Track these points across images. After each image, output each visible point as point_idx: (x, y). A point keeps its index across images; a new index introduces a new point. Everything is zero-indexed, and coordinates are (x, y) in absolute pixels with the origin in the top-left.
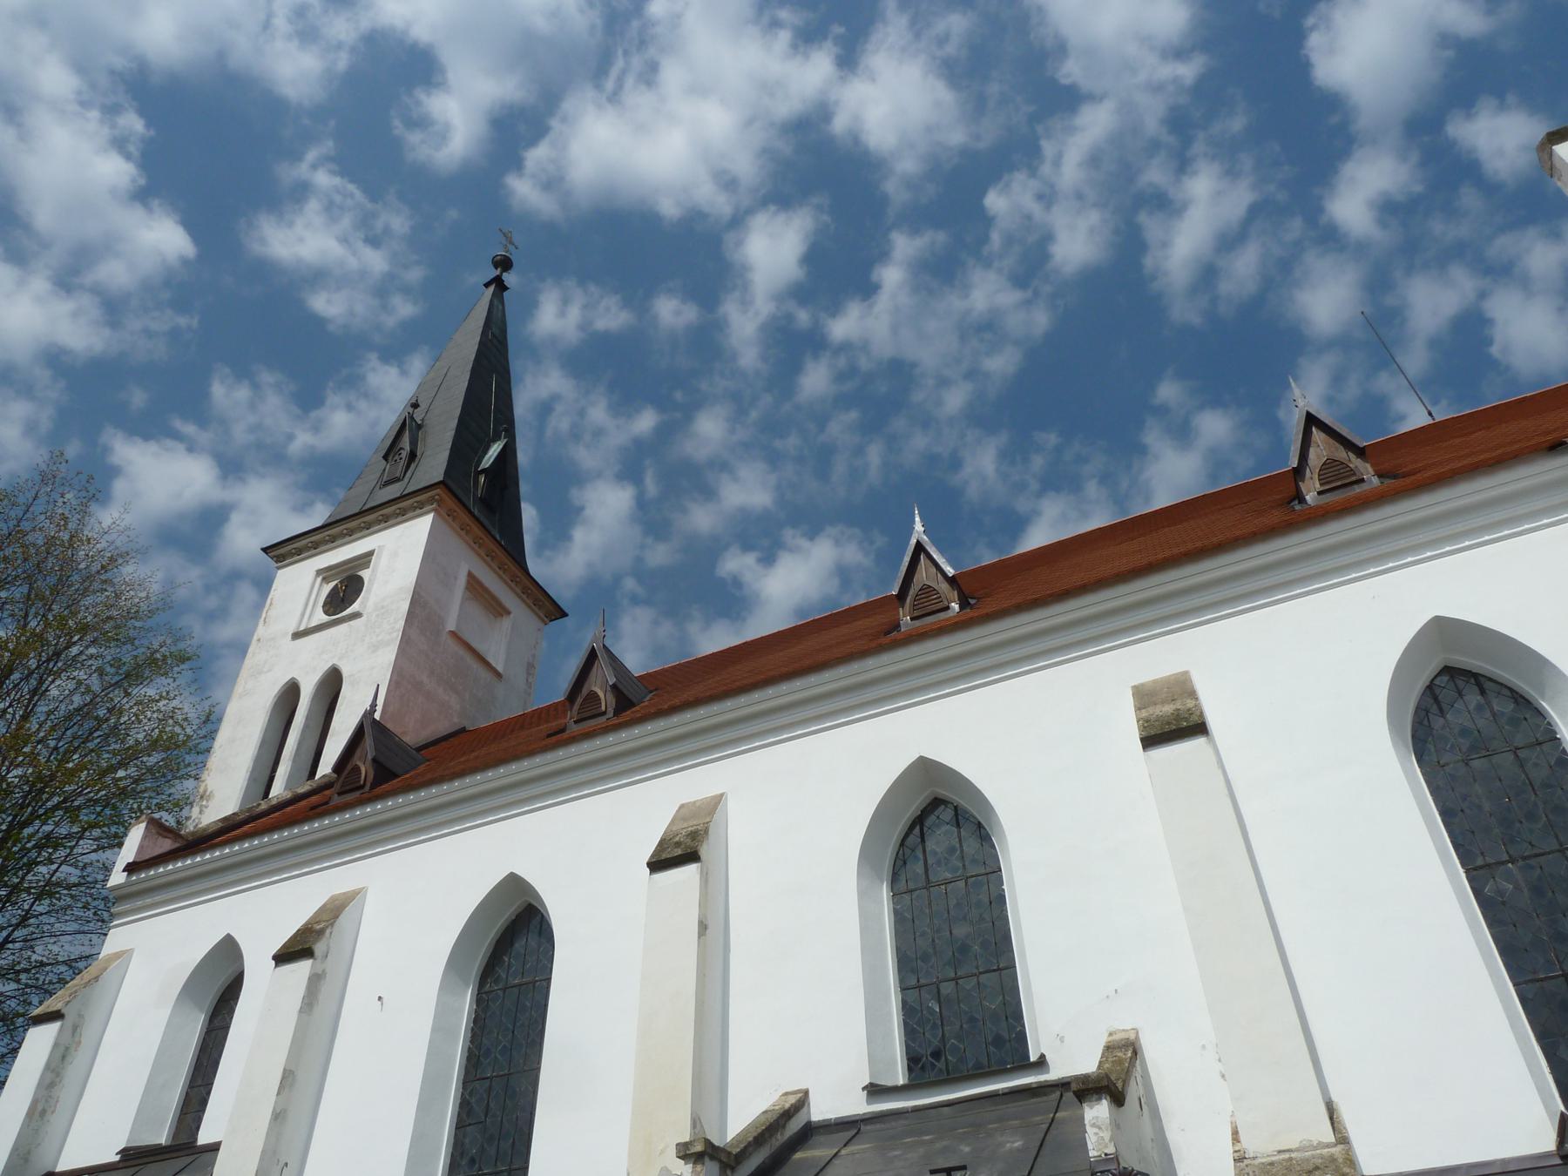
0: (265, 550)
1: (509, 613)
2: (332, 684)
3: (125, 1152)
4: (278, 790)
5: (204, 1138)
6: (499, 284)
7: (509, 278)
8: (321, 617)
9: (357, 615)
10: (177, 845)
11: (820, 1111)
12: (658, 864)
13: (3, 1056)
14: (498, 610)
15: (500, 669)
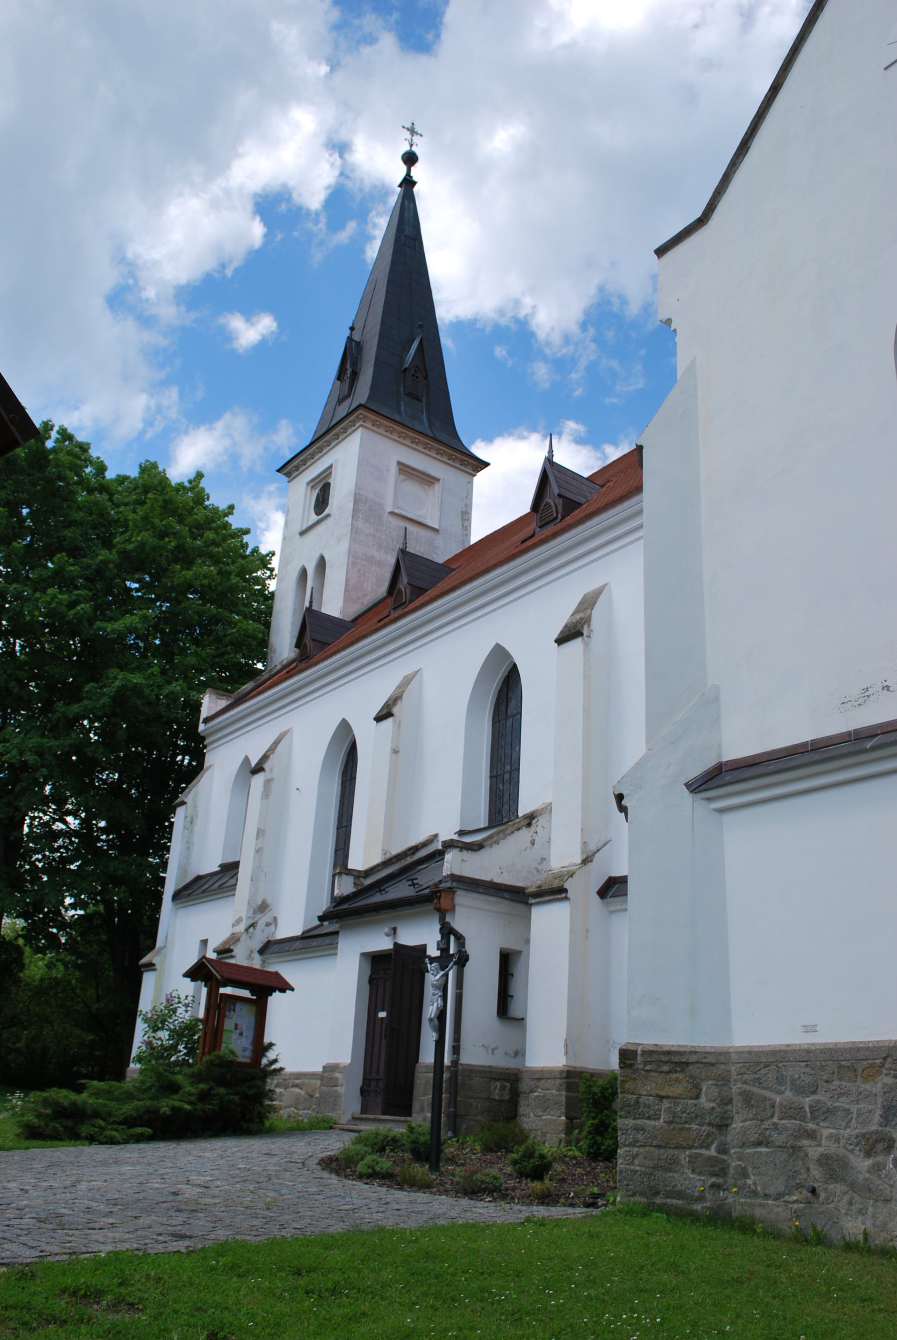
0: (278, 471)
1: (438, 480)
2: (322, 564)
6: (408, 183)
7: (416, 172)
8: (314, 518)
9: (328, 516)
10: (229, 702)
12: (379, 719)
15: (436, 526)
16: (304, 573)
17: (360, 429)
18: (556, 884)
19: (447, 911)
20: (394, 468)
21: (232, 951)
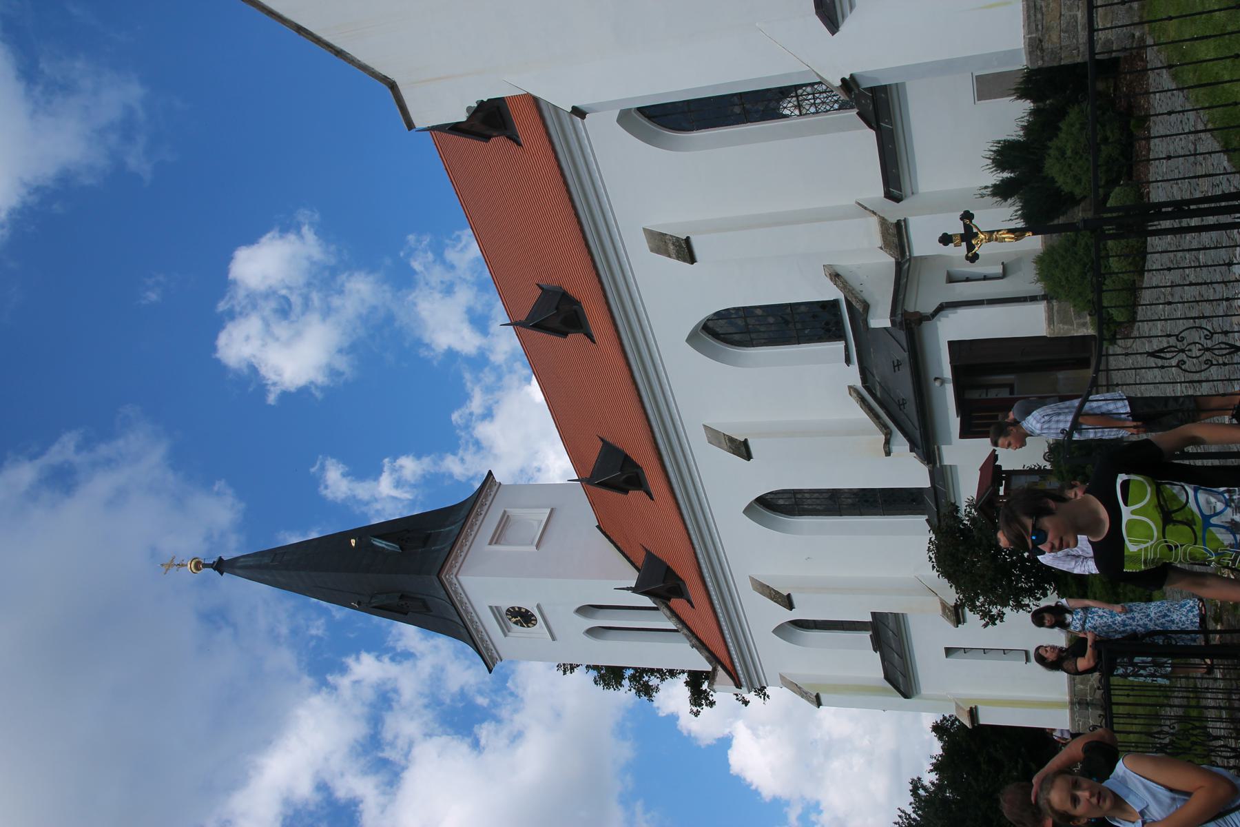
0: (490, 671)
3: (875, 650)
4: (671, 625)
5: (869, 619)
8: (539, 628)
9: (538, 607)
11: (853, 375)
13: (1144, 823)
14: (505, 520)
16: (592, 632)
17: (460, 577)
18: (893, 231)
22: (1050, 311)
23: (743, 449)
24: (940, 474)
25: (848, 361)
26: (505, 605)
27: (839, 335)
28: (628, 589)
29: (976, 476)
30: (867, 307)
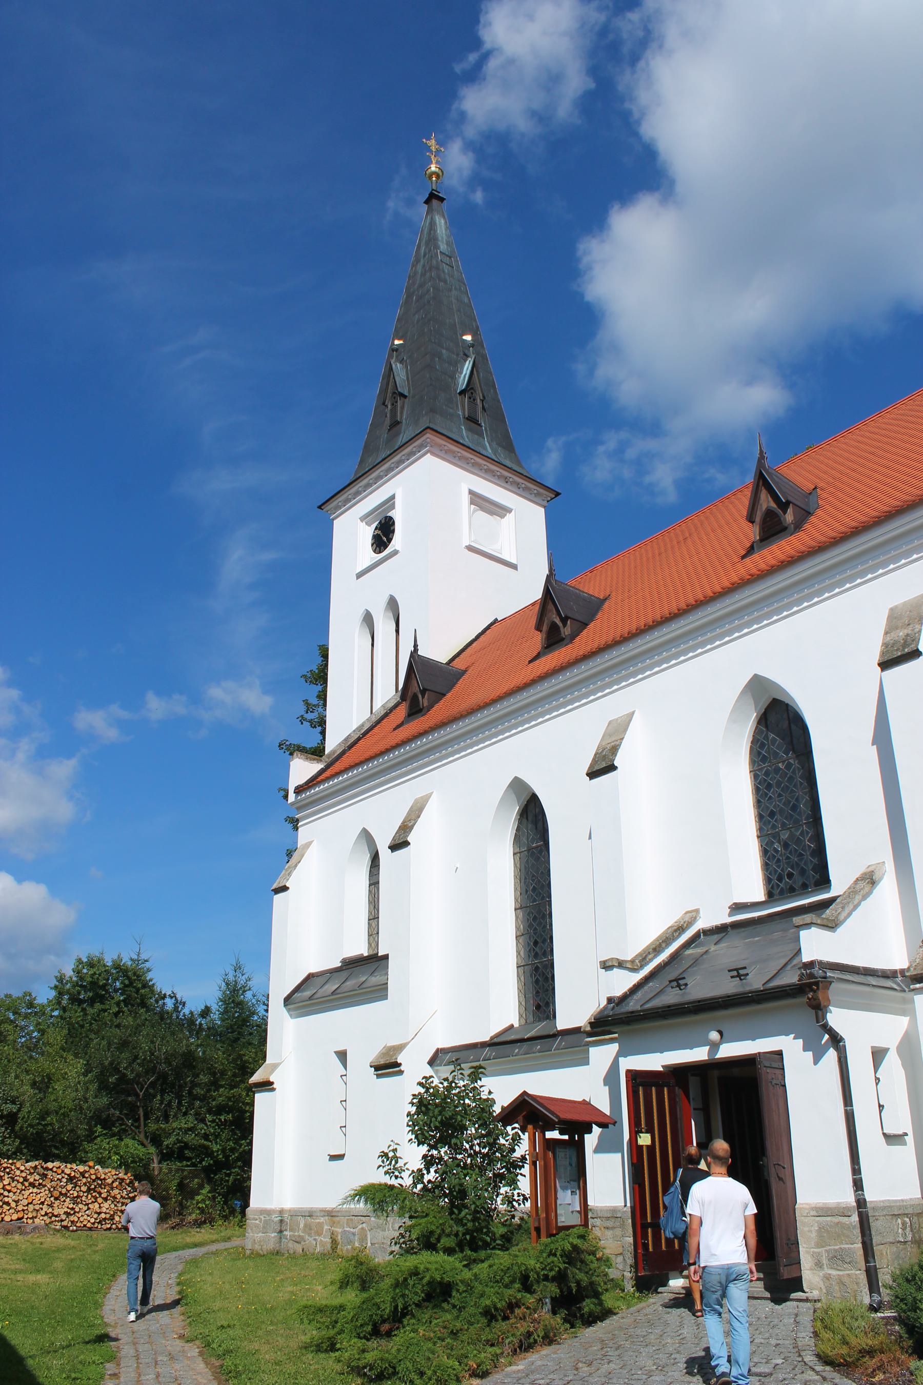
9: (396, 552)
12: (593, 774)
15: (514, 561)
19: (595, 1251)
20: (466, 498)
21: (400, 1065)
22: (843, 1212)
23: (604, 765)
24: (569, 1046)
25: (737, 908)
26: (397, 515)
27: (772, 896)
28: (416, 646)
29: (576, 1096)
30: (831, 926)
